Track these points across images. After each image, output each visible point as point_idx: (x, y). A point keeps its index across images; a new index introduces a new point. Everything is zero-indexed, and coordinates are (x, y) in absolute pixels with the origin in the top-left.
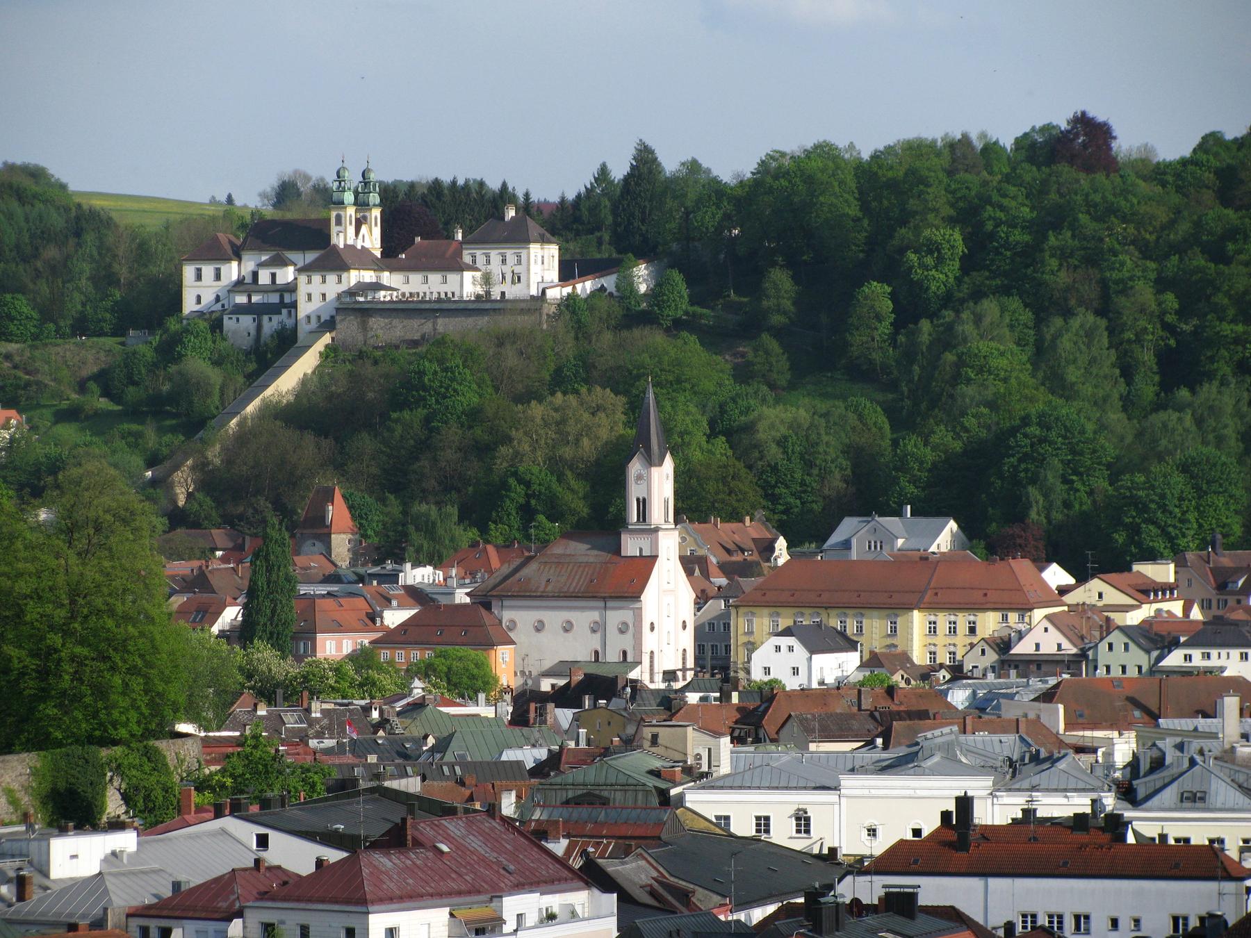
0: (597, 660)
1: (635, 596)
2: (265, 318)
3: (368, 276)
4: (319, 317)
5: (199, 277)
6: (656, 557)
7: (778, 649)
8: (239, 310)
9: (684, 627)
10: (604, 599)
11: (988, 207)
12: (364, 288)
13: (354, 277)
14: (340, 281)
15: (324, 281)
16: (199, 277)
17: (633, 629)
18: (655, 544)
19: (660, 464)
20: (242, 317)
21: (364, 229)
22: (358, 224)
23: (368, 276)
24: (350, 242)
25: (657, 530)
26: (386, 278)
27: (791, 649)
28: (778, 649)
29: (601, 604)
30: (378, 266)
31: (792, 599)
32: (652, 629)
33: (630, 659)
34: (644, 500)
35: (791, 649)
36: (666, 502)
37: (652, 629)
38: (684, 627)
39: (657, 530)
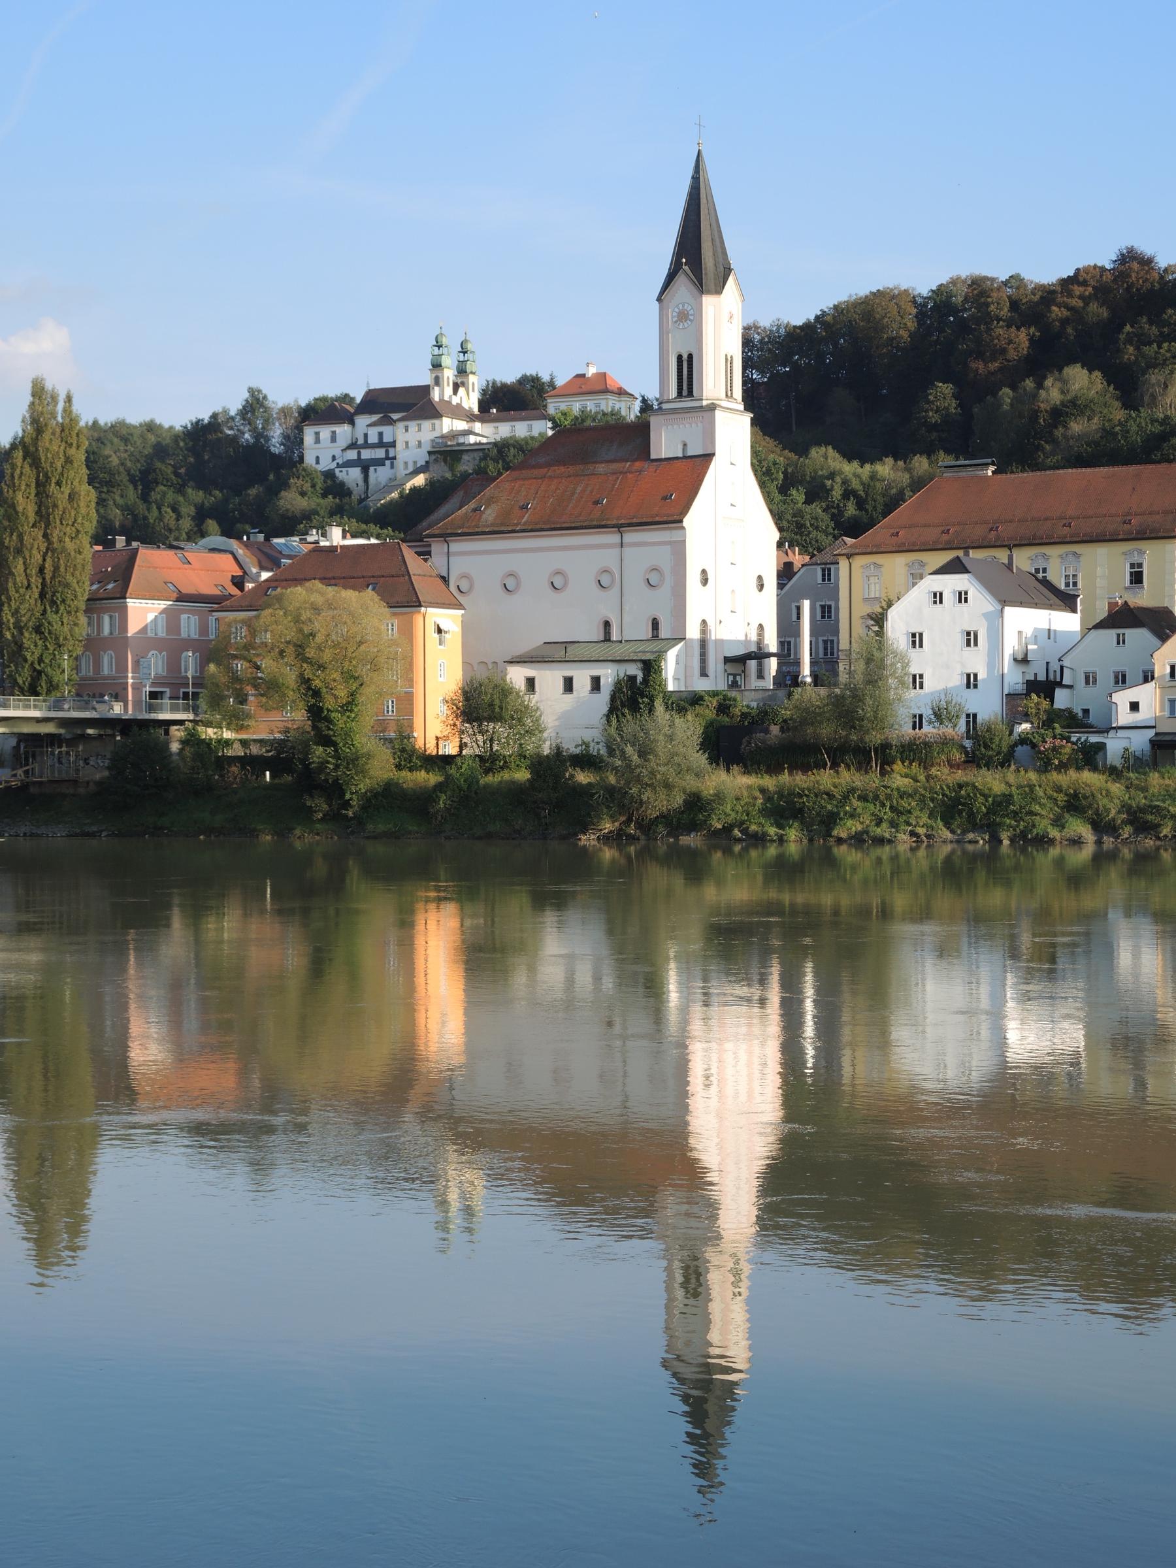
0: (607, 639)
1: (676, 521)
2: (372, 469)
3: (461, 425)
4: (415, 463)
5: (317, 441)
6: (709, 457)
7: (938, 598)
8: (349, 464)
9: (761, 587)
10: (619, 528)
11: (1054, 308)
12: (453, 435)
13: (448, 425)
14: (434, 429)
15: (420, 430)
16: (317, 441)
17: (670, 578)
18: (709, 434)
19: (719, 289)
20: (350, 469)
21: (461, 390)
22: (456, 387)
23: (461, 425)
24: (446, 398)
25: (712, 408)
26: (478, 427)
27: (962, 597)
28: (938, 598)
29: (614, 538)
30: (471, 418)
31: (945, 537)
32: (705, 581)
33: (663, 634)
34: (690, 357)
35: (962, 597)
36: (729, 362)
37: (705, 581)
38: (761, 587)
39: (712, 408)
